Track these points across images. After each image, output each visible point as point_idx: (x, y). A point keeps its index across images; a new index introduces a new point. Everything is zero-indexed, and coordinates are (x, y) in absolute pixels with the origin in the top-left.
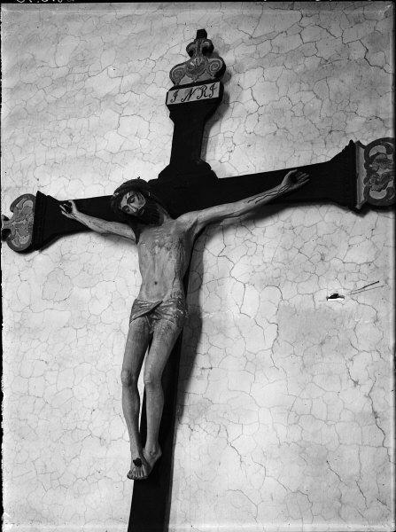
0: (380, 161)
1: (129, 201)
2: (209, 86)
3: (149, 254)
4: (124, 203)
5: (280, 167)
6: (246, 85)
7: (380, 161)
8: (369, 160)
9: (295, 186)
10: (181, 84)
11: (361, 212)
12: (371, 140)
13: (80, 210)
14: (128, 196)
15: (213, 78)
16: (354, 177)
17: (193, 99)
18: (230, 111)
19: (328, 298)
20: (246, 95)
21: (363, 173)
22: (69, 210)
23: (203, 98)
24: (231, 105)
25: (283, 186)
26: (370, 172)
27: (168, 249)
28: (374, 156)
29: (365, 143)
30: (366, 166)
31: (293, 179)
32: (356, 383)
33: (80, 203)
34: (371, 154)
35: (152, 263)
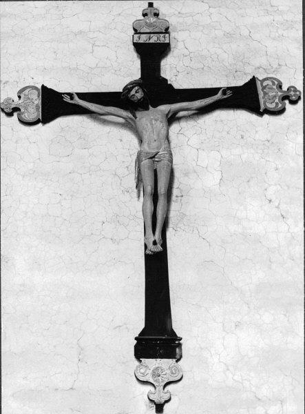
0: (269, 88)
1: (136, 92)
2: (162, 35)
3: (149, 124)
4: (133, 92)
5: (219, 86)
6: (180, 39)
7: (269, 88)
8: (264, 88)
9: (225, 97)
10: (141, 31)
11: (261, 114)
12: (265, 76)
13: (80, 98)
14: (136, 88)
15: (164, 31)
16: (257, 95)
17: (152, 41)
18: (171, 52)
19: (164, 389)
20: (180, 45)
21: (261, 95)
22: (72, 98)
23: (159, 42)
24: (172, 49)
25: (219, 96)
26: (265, 94)
27: (161, 122)
28: (266, 86)
29: (261, 78)
30: (262, 90)
31: (224, 93)
32: (270, 201)
33: (78, 94)
34: (264, 85)
35: (151, 130)
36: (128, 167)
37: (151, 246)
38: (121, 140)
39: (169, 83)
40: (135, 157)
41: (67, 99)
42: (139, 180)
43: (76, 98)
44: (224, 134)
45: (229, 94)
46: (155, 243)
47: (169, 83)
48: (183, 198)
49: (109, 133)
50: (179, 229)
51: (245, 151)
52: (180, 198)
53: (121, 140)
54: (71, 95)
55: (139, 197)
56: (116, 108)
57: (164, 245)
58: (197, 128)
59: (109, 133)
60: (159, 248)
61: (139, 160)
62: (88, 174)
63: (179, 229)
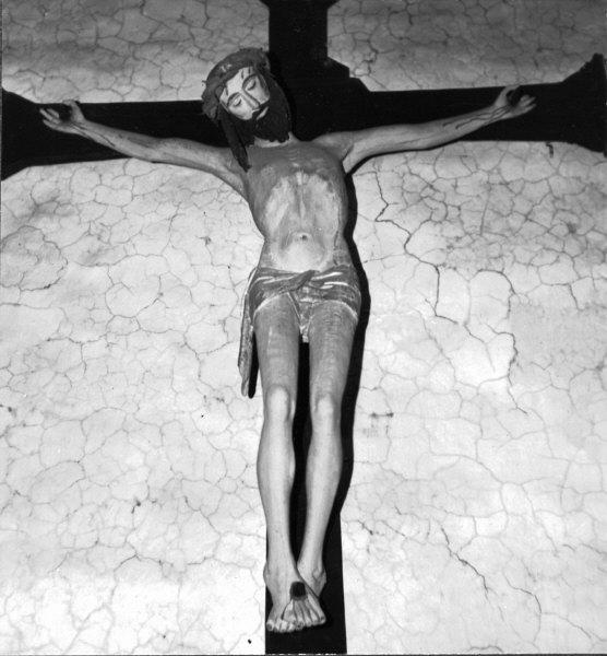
31: (515, 96)
36: (224, 322)
37: (284, 598)
38: (208, 240)
39: (291, 140)
40: (243, 291)
41: (52, 121)
42: (253, 366)
43: (79, 117)
44: (515, 222)
45: (525, 105)
46: (298, 590)
47: (352, 76)
48: (393, 420)
49: (172, 219)
50: (381, 528)
51: (584, 271)
52: (384, 421)
53: (208, 240)
54: (64, 111)
55: (251, 393)
56: (555, 81)
57: (332, 597)
58: (433, 205)
59: (172, 219)
60: (314, 615)
61: (253, 299)
62: (103, 342)
63: (381, 528)
